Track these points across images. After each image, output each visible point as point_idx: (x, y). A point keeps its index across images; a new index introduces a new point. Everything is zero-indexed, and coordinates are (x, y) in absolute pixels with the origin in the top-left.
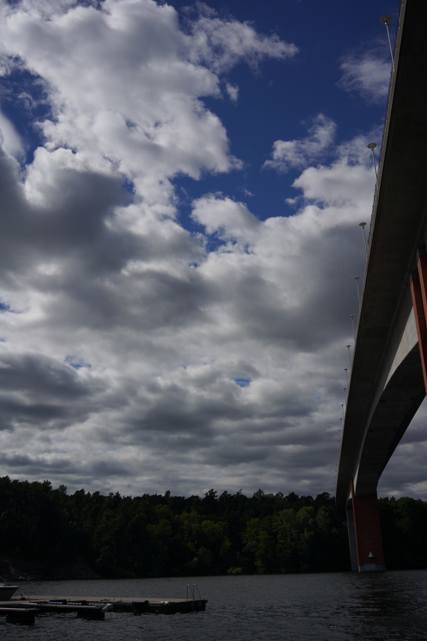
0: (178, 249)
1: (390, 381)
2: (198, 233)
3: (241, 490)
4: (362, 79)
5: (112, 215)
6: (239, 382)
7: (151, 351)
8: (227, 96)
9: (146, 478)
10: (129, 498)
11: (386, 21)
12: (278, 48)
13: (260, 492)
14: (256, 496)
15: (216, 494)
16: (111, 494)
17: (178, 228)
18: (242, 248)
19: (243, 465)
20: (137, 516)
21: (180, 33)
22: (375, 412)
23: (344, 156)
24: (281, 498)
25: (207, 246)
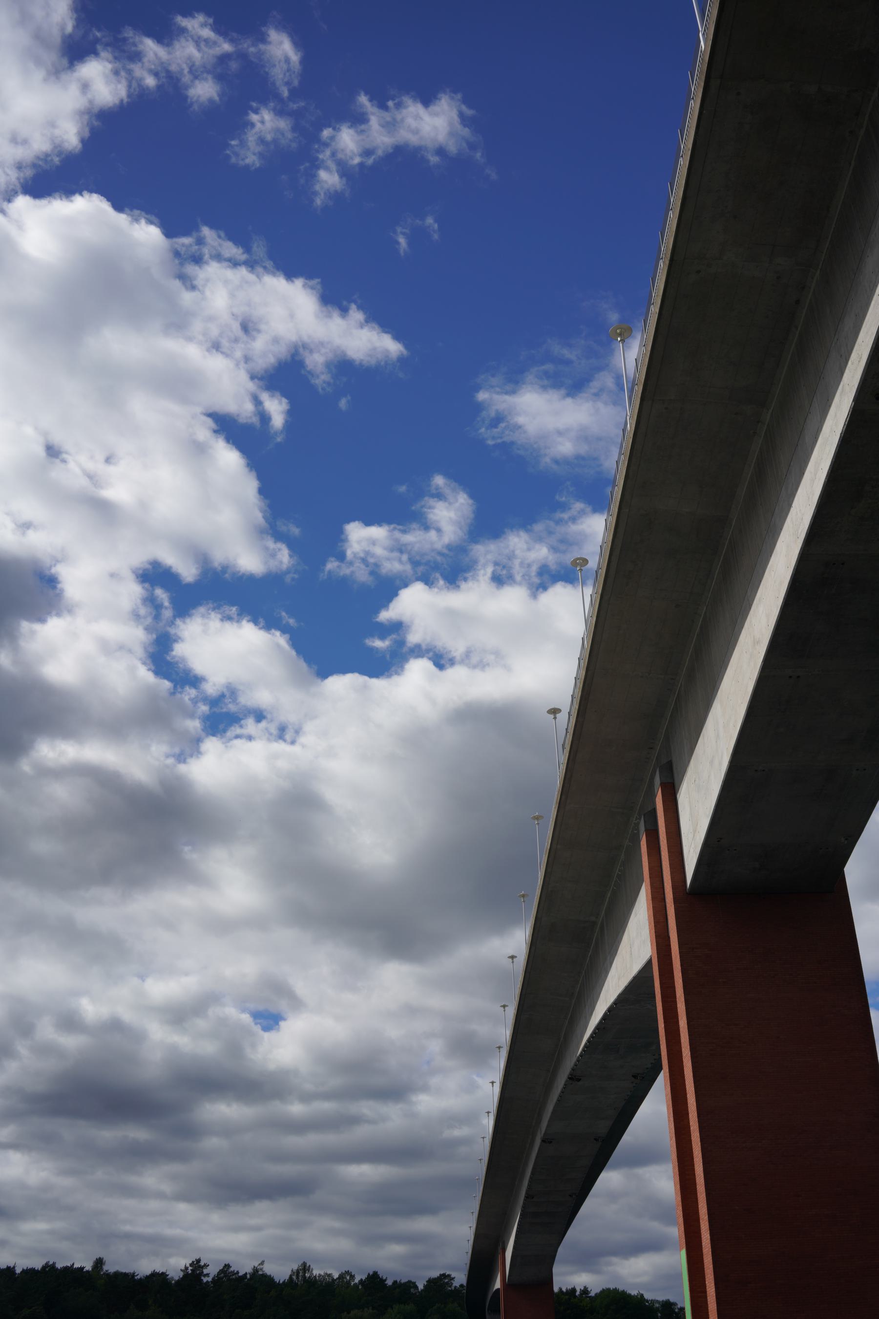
0: (148, 717)
1: (591, 1036)
2: (187, 688)
3: (262, 1263)
4: (521, 420)
6: (259, 1021)
7: (71, 938)
8: (265, 418)
9: (41, 1226)
11: (620, 335)
12: (361, 339)
13: (305, 1268)
14: (294, 1277)
15: (205, 1271)
17: (145, 675)
18: (274, 730)
19: (262, 1205)
21: (177, 283)
22: (558, 1100)
23: (484, 566)
24: (348, 1283)
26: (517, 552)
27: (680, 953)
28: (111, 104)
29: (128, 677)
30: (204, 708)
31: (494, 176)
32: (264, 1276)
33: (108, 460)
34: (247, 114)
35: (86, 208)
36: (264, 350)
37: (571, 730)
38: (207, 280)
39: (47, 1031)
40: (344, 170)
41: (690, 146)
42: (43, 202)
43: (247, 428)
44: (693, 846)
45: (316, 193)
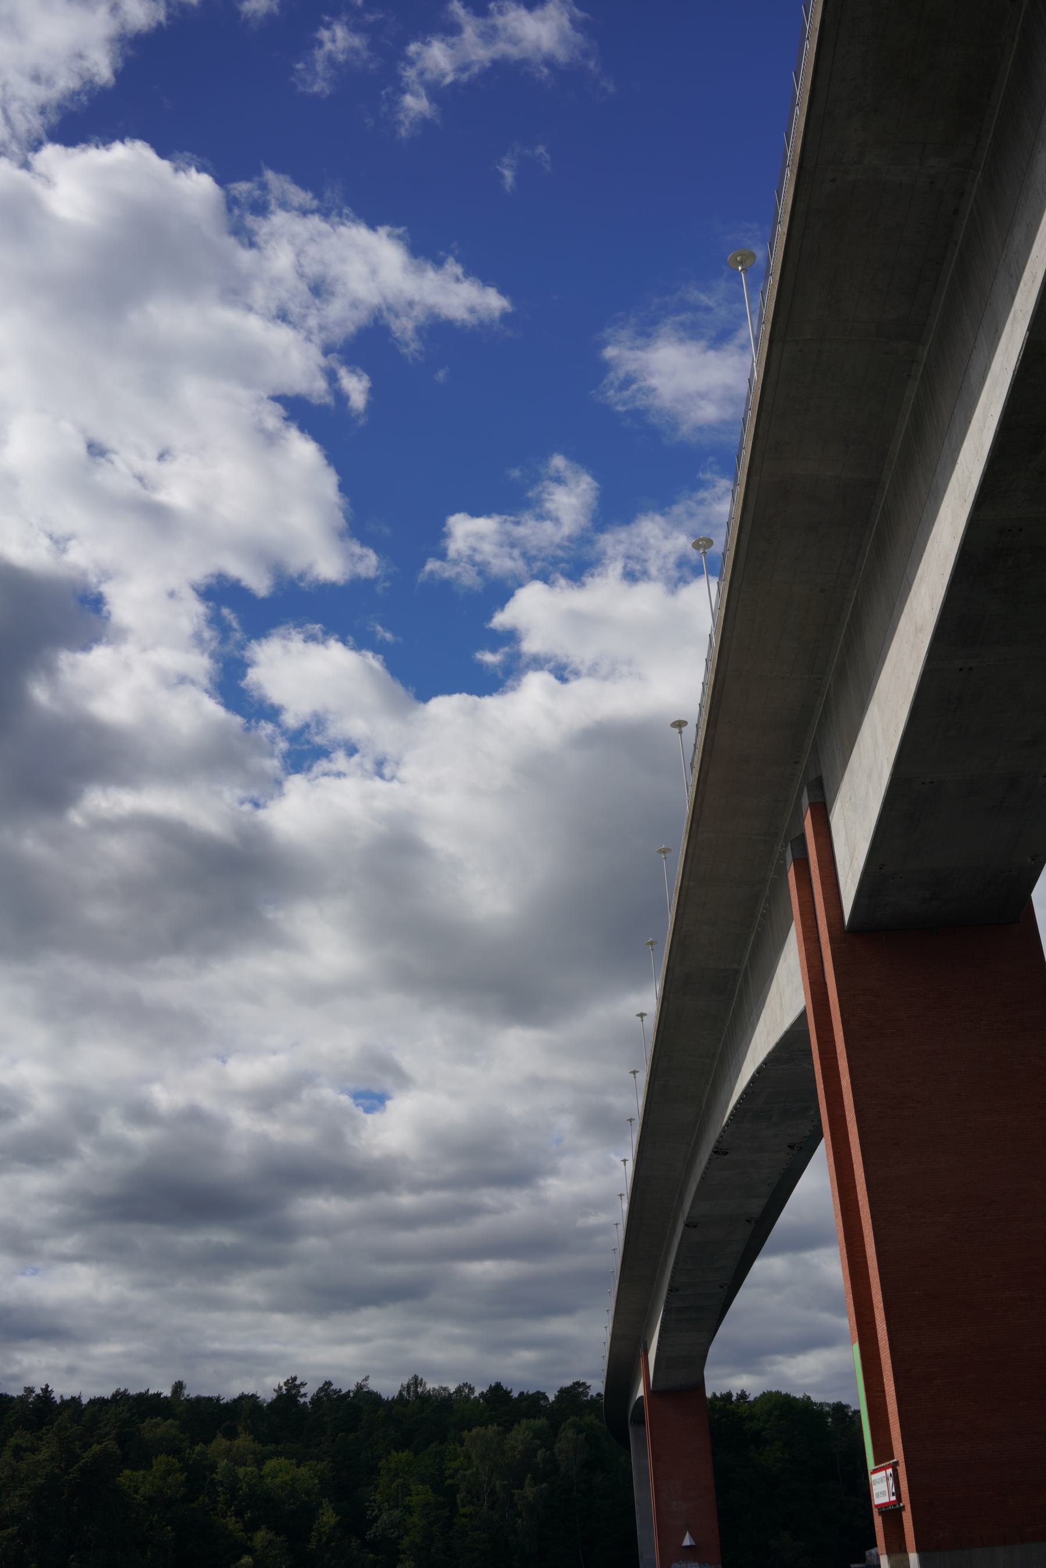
0: (214, 759)
1: (738, 1102)
2: (263, 723)
3: (366, 1379)
4: (654, 382)
5: (51, 671)
6: (361, 1101)
7: (137, 1016)
8: (341, 397)
9: (115, 1348)
10: (75, 1401)
11: (741, 263)
12: (460, 296)
13: (416, 1382)
14: (405, 1393)
15: (303, 1391)
16: (29, 1390)
17: (213, 709)
18: (369, 766)
19: (369, 1312)
20: (96, 1448)
21: (231, 242)
22: (702, 1178)
23: (614, 559)
24: (467, 1397)
25: (287, 756)
26: (652, 541)
27: (839, 1001)
28: (146, 29)
29: (194, 713)
30: (283, 745)
31: (611, 89)
32: (370, 1393)
33: (162, 457)
34: (317, 30)
35: (128, 158)
36: (339, 315)
37: (700, 746)
38: (271, 234)
39: (114, 1124)
40: (435, 91)
41: (817, 25)
42: (71, 150)
43: (323, 409)
44: (850, 876)
45: (401, 123)
